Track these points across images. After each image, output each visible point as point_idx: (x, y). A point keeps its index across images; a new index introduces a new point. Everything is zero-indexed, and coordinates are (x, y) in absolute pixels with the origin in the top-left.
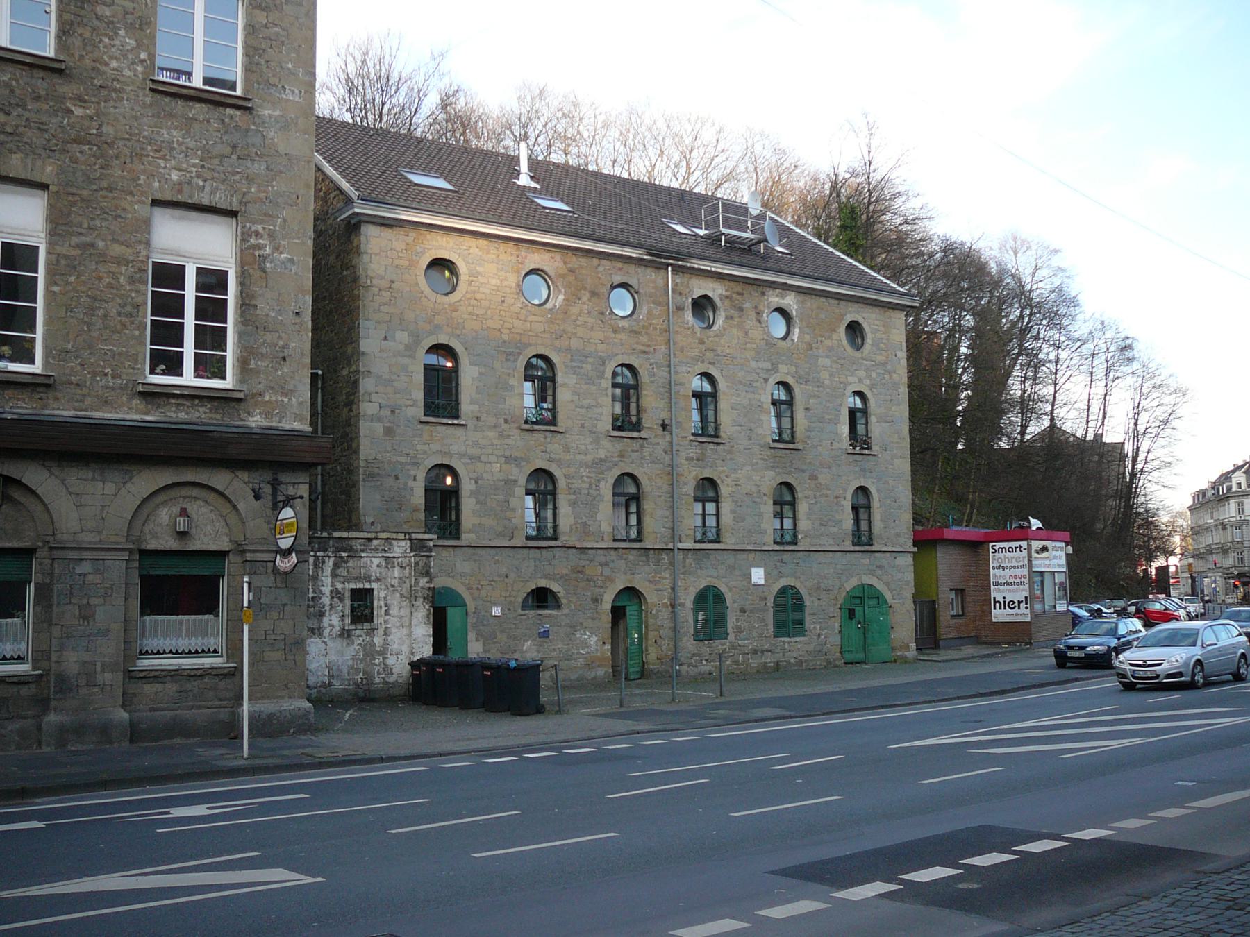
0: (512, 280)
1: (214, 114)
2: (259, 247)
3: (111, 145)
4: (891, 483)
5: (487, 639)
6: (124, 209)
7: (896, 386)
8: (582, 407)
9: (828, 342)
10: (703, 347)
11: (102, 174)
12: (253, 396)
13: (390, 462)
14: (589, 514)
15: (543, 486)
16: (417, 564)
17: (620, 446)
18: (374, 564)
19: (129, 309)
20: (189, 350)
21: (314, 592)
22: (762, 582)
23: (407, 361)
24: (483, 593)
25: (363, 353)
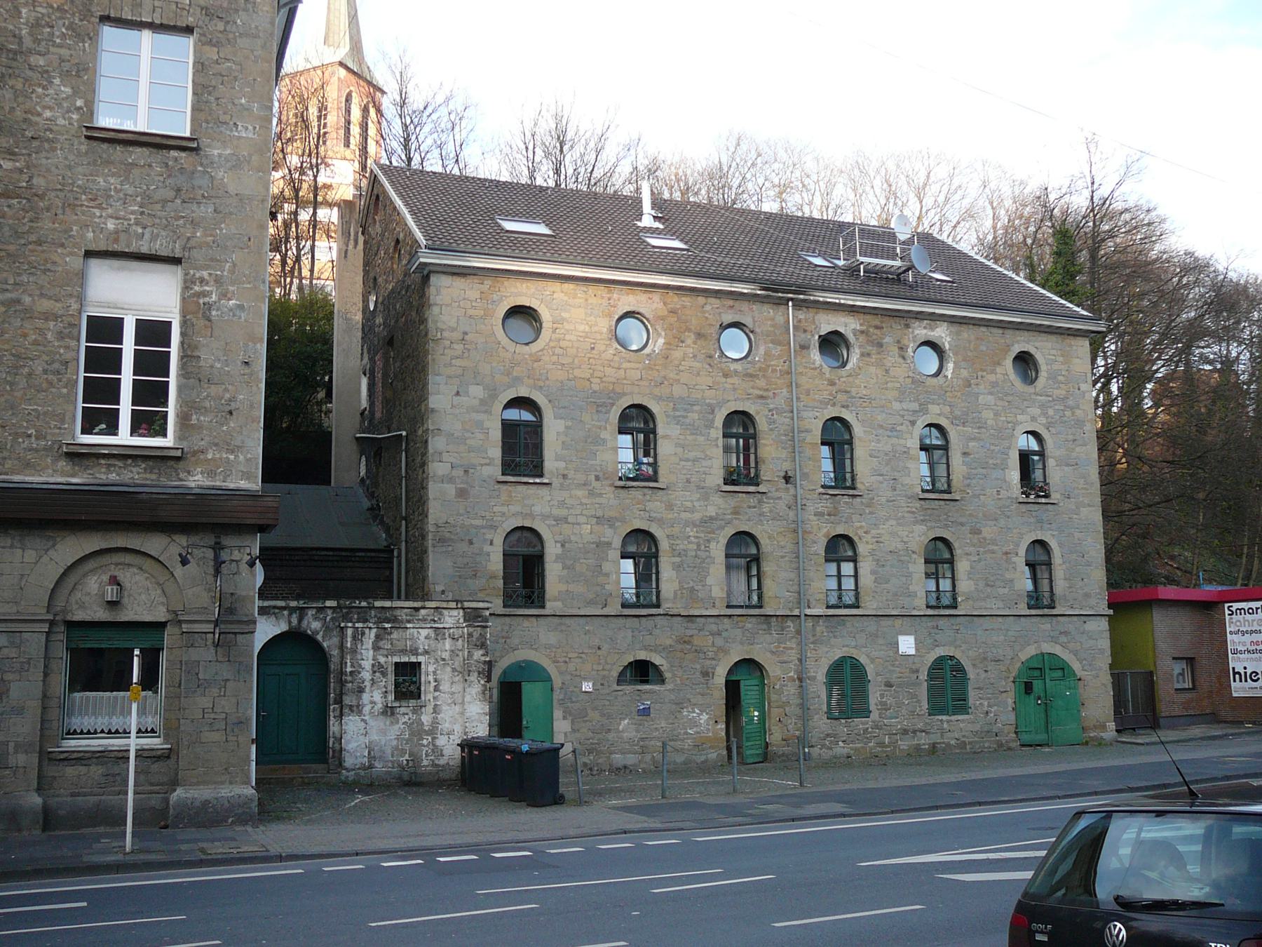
0: (604, 325)
1: (156, 158)
2: (204, 294)
3: (41, 197)
4: (1077, 535)
5: (578, 717)
6: (54, 263)
7: (1080, 423)
8: (687, 460)
9: (992, 378)
10: (834, 389)
11: (31, 227)
12: (195, 453)
14: (697, 575)
15: (643, 548)
16: (470, 635)
17: (733, 501)
18: (421, 635)
19: (56, 366)
20: (126, 407)
21: (352, 666)
22: (913, 652)
24: (571, 667)
25: (433, 410)
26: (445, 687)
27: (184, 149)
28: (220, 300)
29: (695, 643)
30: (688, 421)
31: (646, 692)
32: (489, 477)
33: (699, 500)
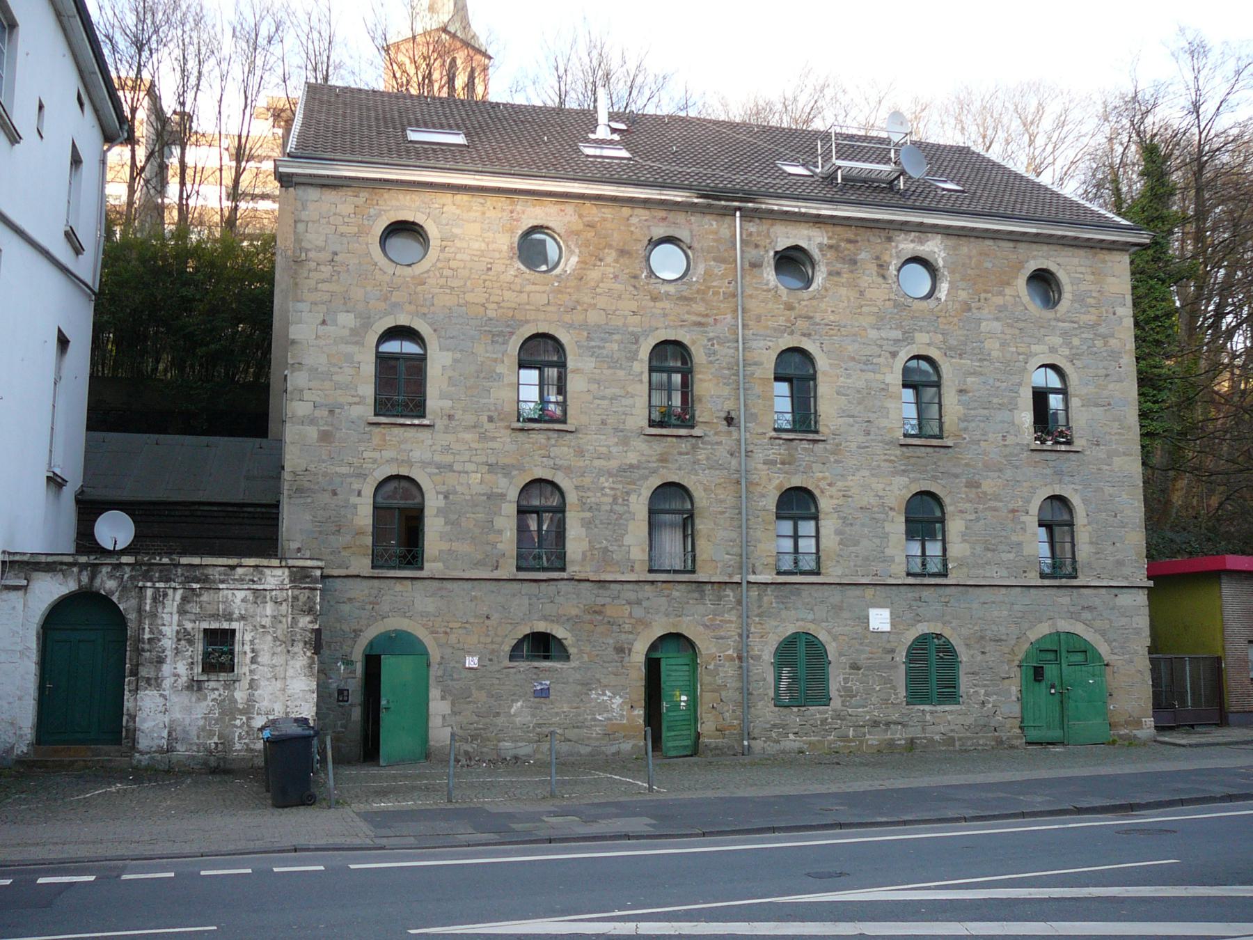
5: (459, 698)
13: (325, 475)
16: (295, 598)
17: (658, 447)
18: (237, 598)
21: (151, 632)
23: (355, 349)
24: (453, 638)
26: (264, 658)
30: (605, 352)
31: (549, 670)
32: (359, 418)
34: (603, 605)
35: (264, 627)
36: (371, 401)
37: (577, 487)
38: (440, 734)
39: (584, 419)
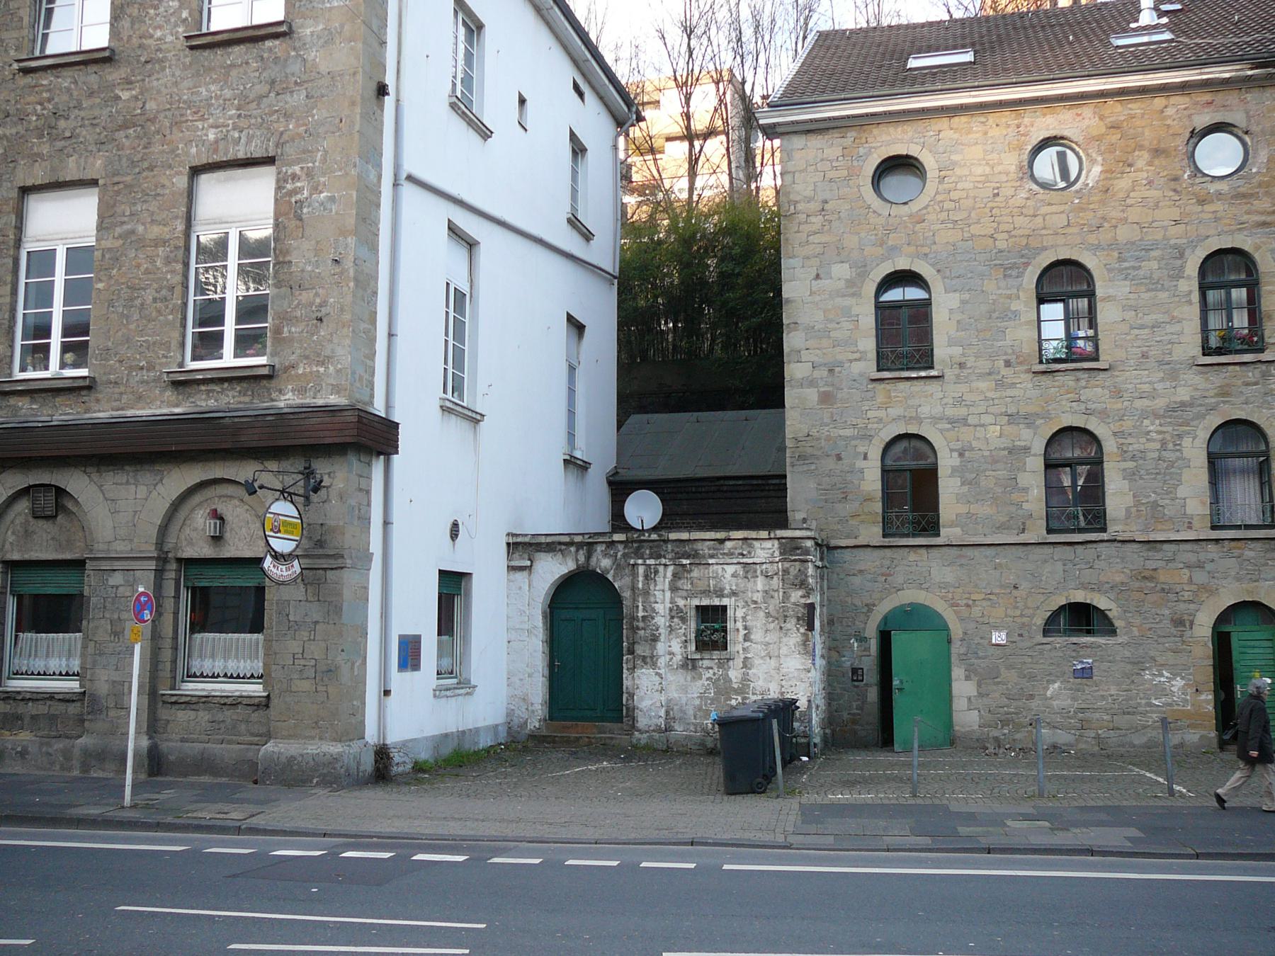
0: (1011, 162)
5: (985, 678)
12: (286, 369)
13: (828, 438)
16: (786, 571)
17: (1218, 378)
18: (727, 573)
19: (164, 292)
21: (645, 610)
23: (849, 301)
24: (976, 612)
25: (788, 301)
26: (757, 635)
27: (276, 36)
28: (311, 195)
29: (1162, 579)
30: (1141, 272)
31: (1086, 646)
32: (861, 375)
33: (1162, 380)
34: (1155, 570)
35: (755, 602)
36: (873, 355)
37: (1115, 434)
38: (967, 717)
39: (1120, 354)
